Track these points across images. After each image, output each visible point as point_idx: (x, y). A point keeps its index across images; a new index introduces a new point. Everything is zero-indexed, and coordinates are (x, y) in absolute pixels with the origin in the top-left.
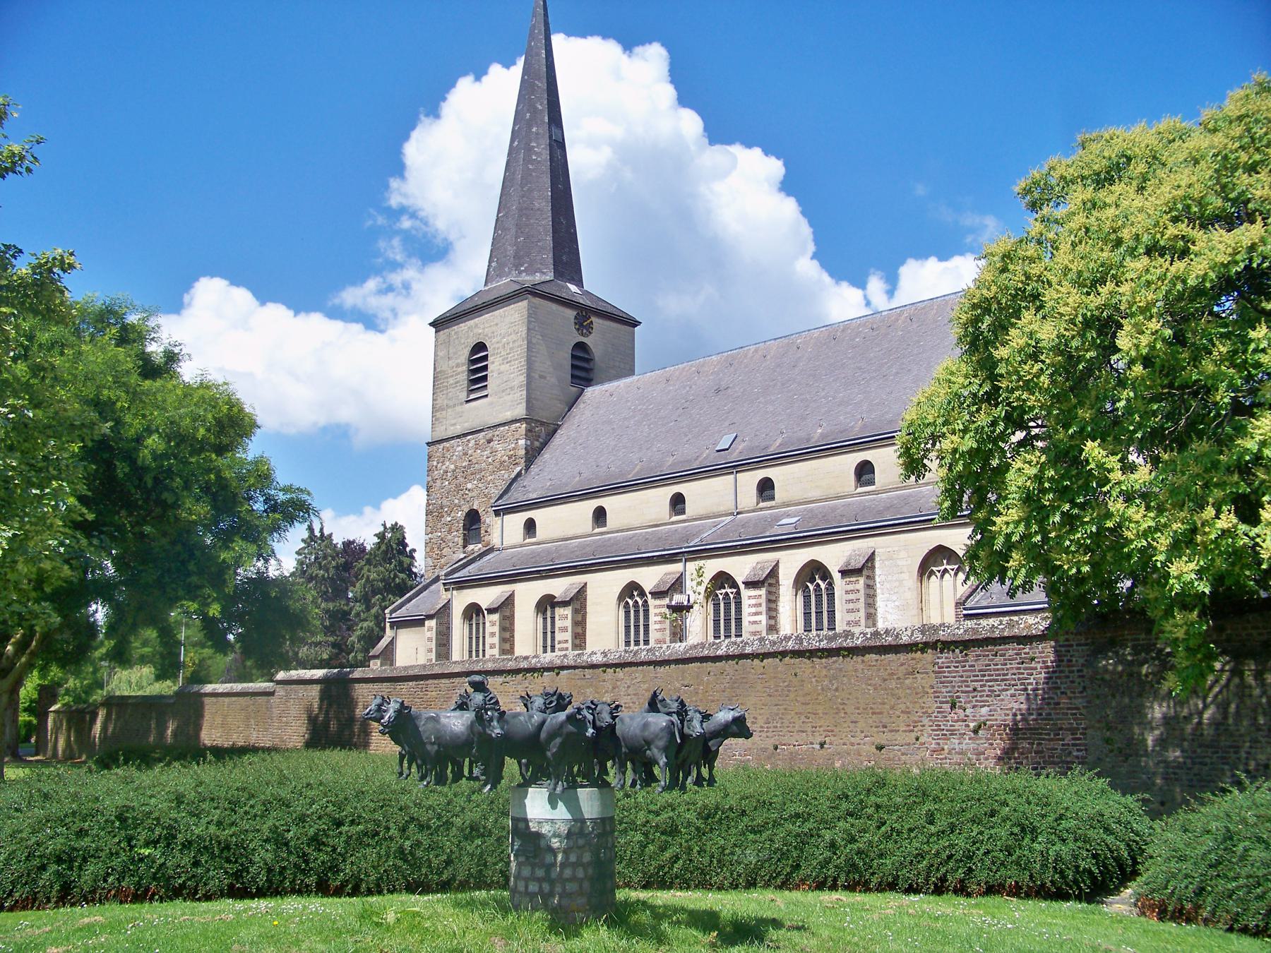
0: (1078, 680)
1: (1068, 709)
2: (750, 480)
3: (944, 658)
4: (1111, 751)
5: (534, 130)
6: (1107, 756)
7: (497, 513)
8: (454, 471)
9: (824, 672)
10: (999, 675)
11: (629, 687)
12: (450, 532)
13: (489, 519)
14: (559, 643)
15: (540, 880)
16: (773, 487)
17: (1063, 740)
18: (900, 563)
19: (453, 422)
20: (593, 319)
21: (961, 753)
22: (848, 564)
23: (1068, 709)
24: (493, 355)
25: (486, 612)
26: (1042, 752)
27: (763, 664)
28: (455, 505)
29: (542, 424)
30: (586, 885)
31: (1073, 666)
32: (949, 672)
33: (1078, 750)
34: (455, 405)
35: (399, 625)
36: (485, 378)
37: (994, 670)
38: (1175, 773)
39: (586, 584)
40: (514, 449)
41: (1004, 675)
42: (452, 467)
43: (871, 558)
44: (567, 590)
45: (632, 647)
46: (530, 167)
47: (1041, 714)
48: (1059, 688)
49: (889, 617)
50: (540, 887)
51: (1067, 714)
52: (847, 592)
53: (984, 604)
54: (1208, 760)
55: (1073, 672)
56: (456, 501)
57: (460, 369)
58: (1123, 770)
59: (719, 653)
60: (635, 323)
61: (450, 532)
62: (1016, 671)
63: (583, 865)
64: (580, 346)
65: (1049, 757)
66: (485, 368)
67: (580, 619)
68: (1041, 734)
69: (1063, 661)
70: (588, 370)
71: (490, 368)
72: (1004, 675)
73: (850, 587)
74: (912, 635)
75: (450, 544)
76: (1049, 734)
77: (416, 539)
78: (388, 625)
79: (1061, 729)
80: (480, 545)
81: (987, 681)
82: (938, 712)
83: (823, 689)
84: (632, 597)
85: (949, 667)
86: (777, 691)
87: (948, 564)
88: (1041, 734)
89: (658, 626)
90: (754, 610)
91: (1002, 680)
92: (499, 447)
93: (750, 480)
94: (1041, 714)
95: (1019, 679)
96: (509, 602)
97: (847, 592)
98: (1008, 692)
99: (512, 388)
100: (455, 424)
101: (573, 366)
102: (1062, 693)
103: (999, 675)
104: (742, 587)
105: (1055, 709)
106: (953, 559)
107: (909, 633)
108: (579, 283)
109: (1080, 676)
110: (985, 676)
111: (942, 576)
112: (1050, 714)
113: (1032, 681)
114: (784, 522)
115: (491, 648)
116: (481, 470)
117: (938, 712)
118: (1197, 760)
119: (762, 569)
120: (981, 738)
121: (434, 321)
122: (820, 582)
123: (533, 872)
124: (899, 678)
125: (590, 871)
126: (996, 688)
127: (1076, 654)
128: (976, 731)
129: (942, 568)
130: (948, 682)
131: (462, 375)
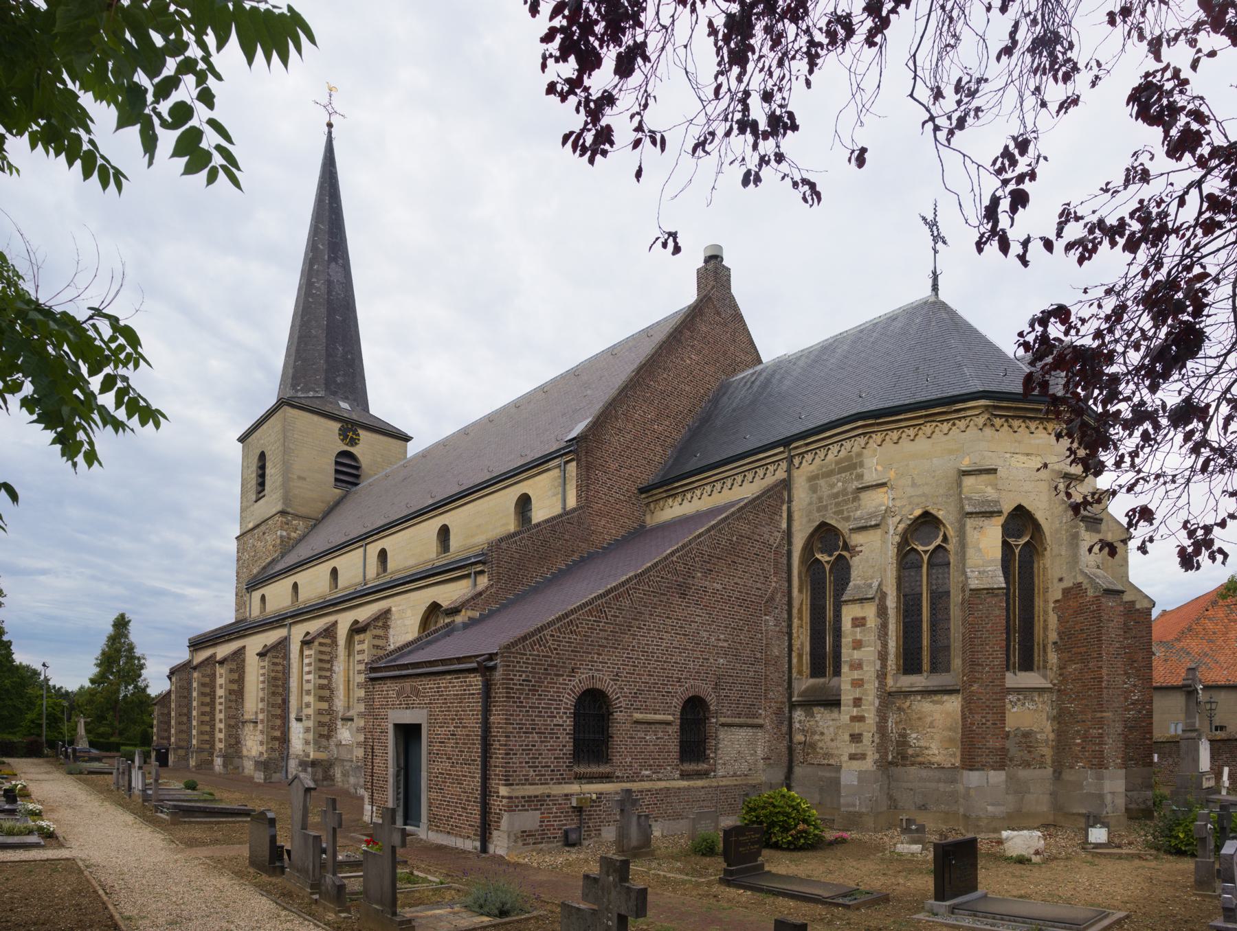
20: (360, 431)
101: (337, 471)
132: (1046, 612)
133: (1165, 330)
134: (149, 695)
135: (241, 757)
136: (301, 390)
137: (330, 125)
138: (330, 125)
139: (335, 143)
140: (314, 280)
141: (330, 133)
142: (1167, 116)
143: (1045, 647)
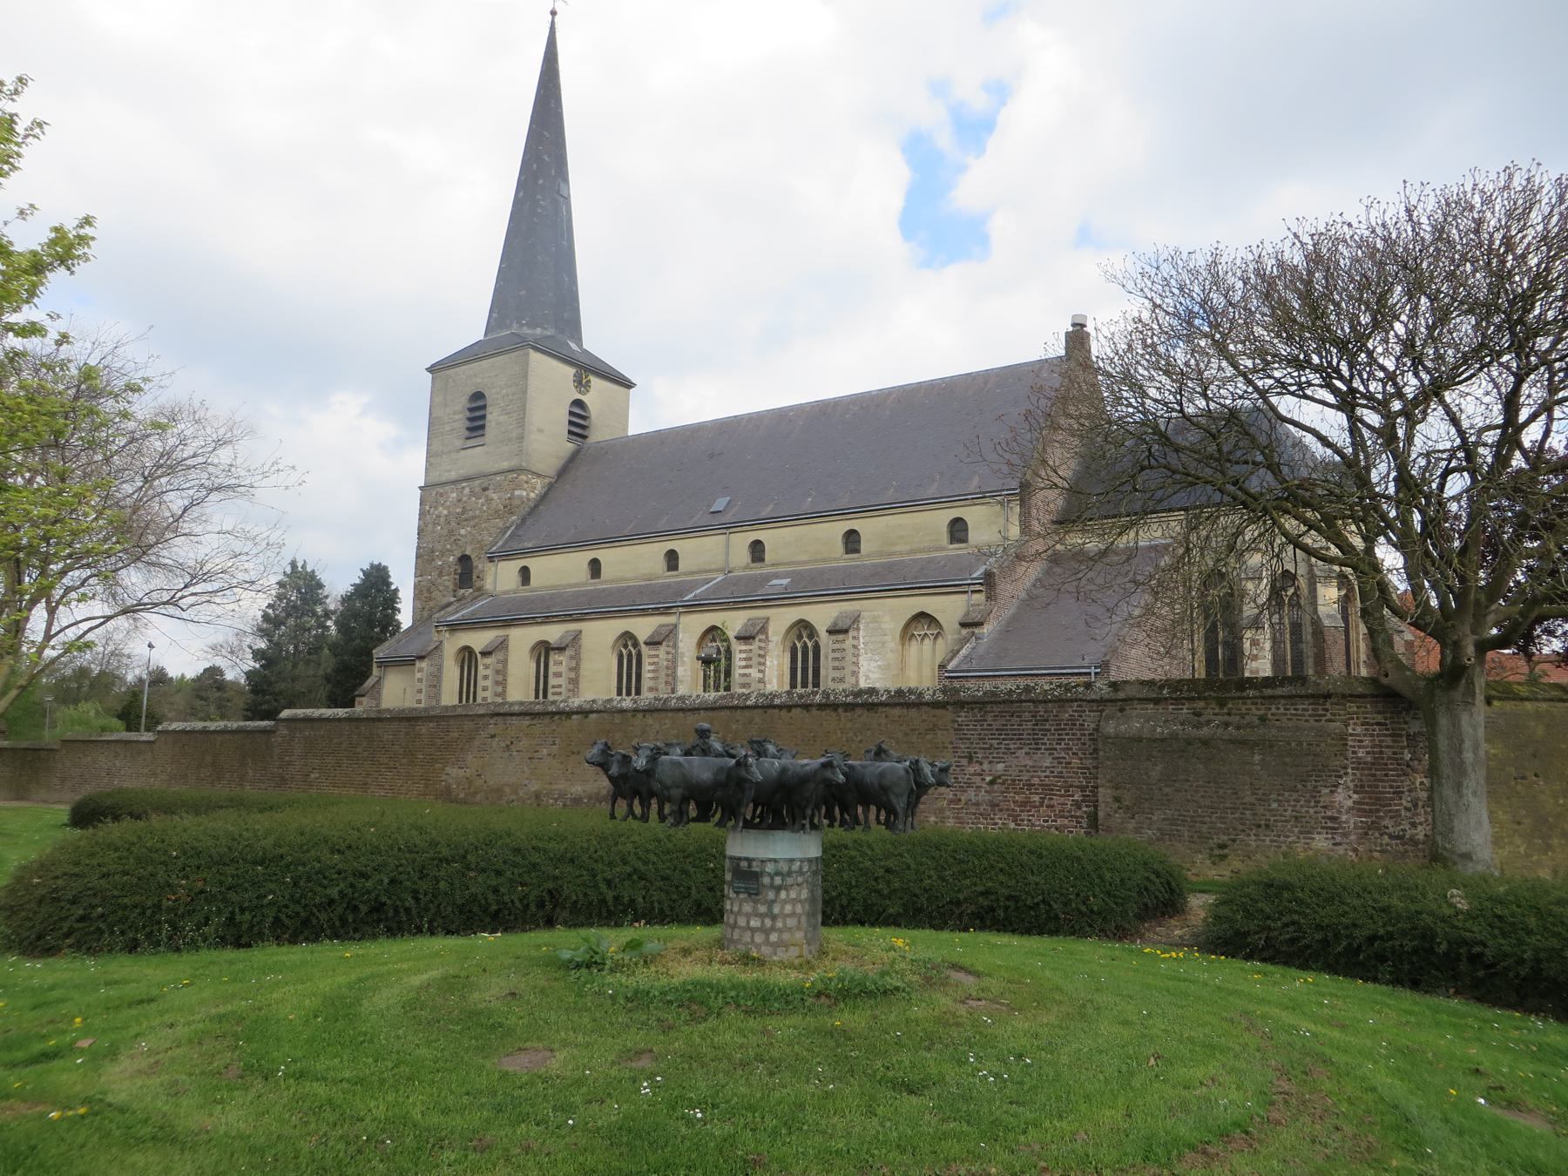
0: (1088, 743)
1: (1079, 768)
2: (742, 541)
3: (962, 717)
4: (1119, 808)
5: (541, 182)
6: (1116, 812)
7: (491, 559)
8: (446, 516)
9: (849, 725)
10: (1015, 735)
11: (658, 732)
12: (440, 575)
13: (479, 564)
14: (553, 687)
15: (762, 916)
16: (677, 558)
17: (1073, 796)
18: (883, 626)
19: (448, 468)
20: (592, 378)
21: (977, 804)
22: (835, 624)
23: (1079, 768)
24: (491, 405)
25: (479, 656)
26: (1053, 806)
27: (791, 714)
28: (448, 550)
29: (539, 475)
30: (803, 919)
31: (1086, 730)
32: (968, 730)
33: (1087, 806)
34: (450, 452)
35: (386, 664)
36: (483, 427)
37: (1011, 730)
38: (1177, 830)
39: (581, 632)
40: (510, 498)
41: (1020, 734)
42: (445, 512)
43: (856, 619)
44: (562, 638)
45: (799, 690)
46: (535, 220)
47: (1052, 772)
48: (1071, 749)
49: (871, 675)
50: (763, 922)
51: (1077, 773)
52: (833, 651)
53: (965, 667)
54: (1207, 819)
55: (1085, 735)
56: (449, 546)
57: (457, 417)
58: (1130, 826)
59: (749, 703)
60: (629, 385)
61: (440, 575)
62: (1030, 732)
63: (800, 901)
64: (578, 403)
65: (1060, 811)
66: (484, 417)
67: (574, 665)
68: (1052, 790)
69: (1075, 725)
70: (584, 427)
71: (489, 417)
72: (1020, 734)
73: (837, 646)
74: (934, 694)
75: (441, 588)
76: (1060, 791)
77: (404, 581)
78: (375, 665)
79: (1071, 786)
80: (471, 590)
81: (1004, 739)
82: (957, 766)
83: (847, 741)
84: (800, 637)
85: (968, 725)
86: (803, 740)
87: (928, 629)
88: (1052, 790)
89: (650, 675)
90: (744, 663)
91: (1019, 739)
92: (495, 496)
93: (742, 541)
94: (1052, 772)
95: (1034, 739)
96: (502, 645)
97: (833, 651)
98: (1023, 751)
99: (510, 440)
100: (449, 471)
101: (571, 423)
102: (1074, 754)
103: (1015, 735)
104: (733, 641)
105: (1066, 768)
106: (933, 624)
107: (931, 692)
108: (579, 341)
109: (1090, 739)
110: (1001, 734)
111: (923, 639)
112: (1062, 772)
113: (1045, 741)
114: (774, 582)
115: (484, 690)
116: (474, 518)
117: (957, 766)
118: (1198, 819)
119: (754, 625)
120: (996, 792)
121: (433, 366)
122: (807, 641)
123: (755, 909)
124: (920, 734)
125: (807, 906)
126: (1012, 746)
127: (1088, 719)
128: (992, 783)
129: (923, 633)
130: (967, 739)
131: (460, 422)
132: (1358, 641)
133: (1537, 312)
134: (250, 675)
135: (1302, 642)
136: (526, 324)
137: (553, 13)
138: (553, 13)
139: (558, 35)
140: (539, 197)
141: (553, 23)
142: (1358, 511)
143: (1358, 663)
